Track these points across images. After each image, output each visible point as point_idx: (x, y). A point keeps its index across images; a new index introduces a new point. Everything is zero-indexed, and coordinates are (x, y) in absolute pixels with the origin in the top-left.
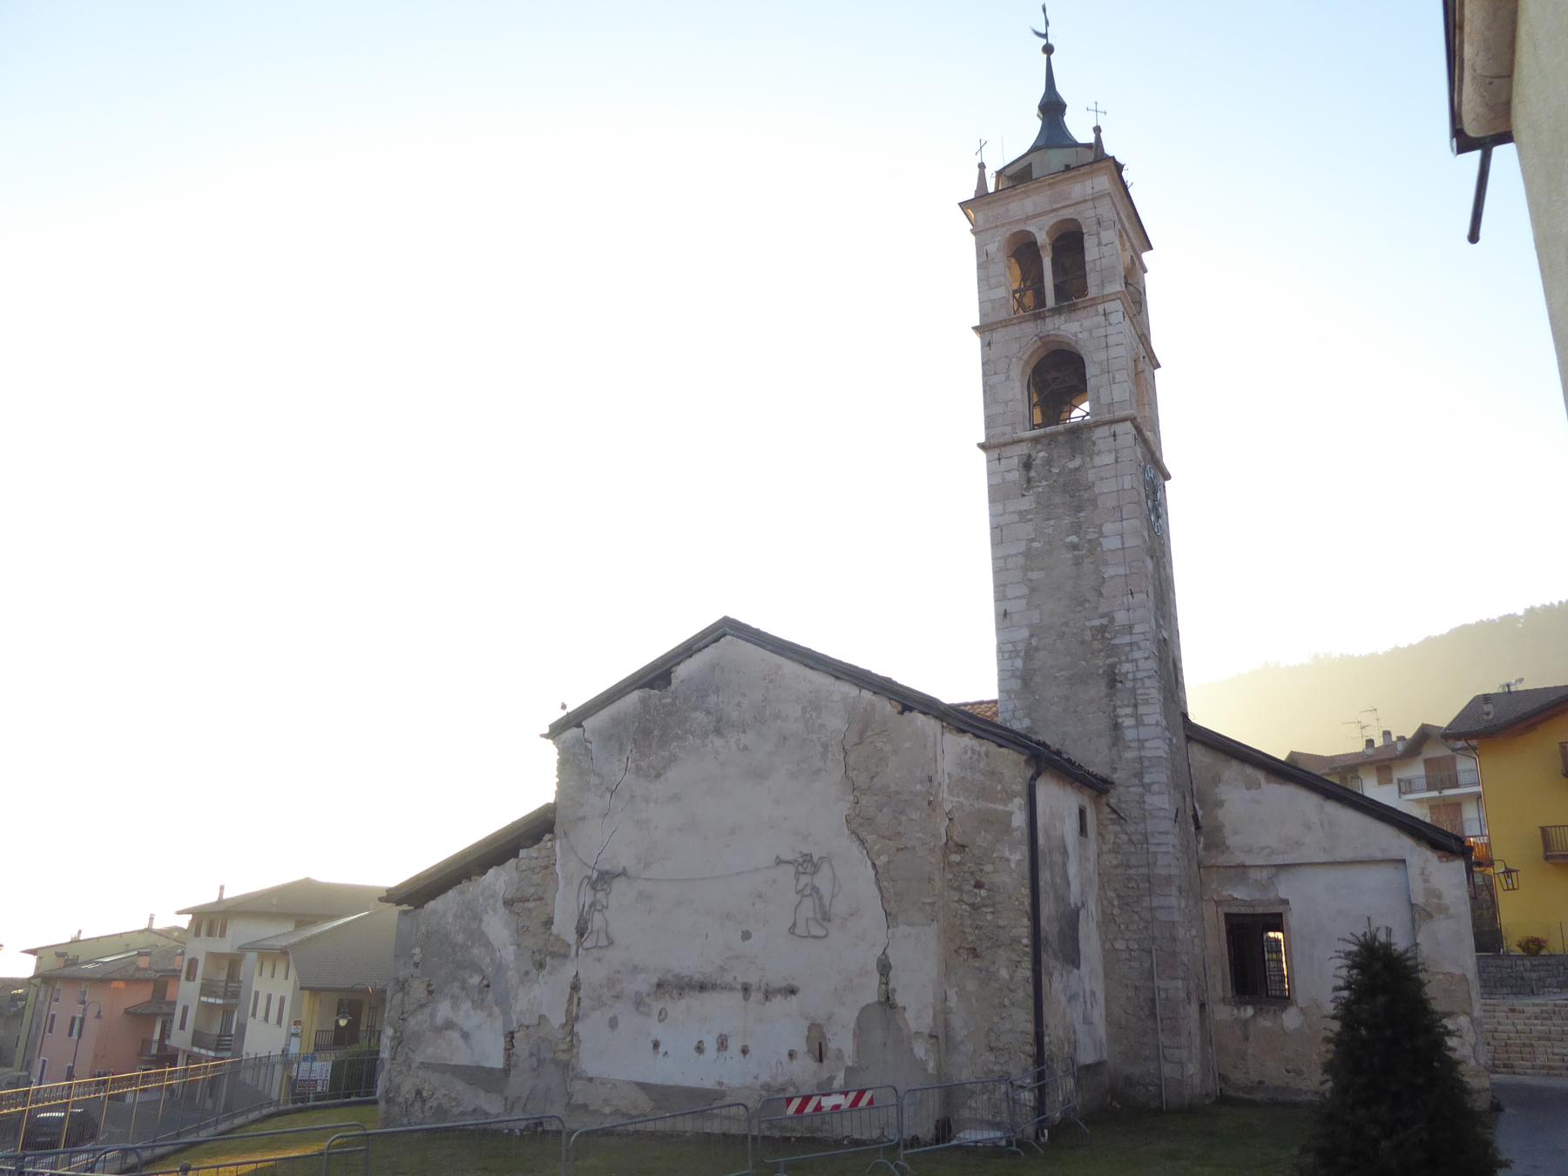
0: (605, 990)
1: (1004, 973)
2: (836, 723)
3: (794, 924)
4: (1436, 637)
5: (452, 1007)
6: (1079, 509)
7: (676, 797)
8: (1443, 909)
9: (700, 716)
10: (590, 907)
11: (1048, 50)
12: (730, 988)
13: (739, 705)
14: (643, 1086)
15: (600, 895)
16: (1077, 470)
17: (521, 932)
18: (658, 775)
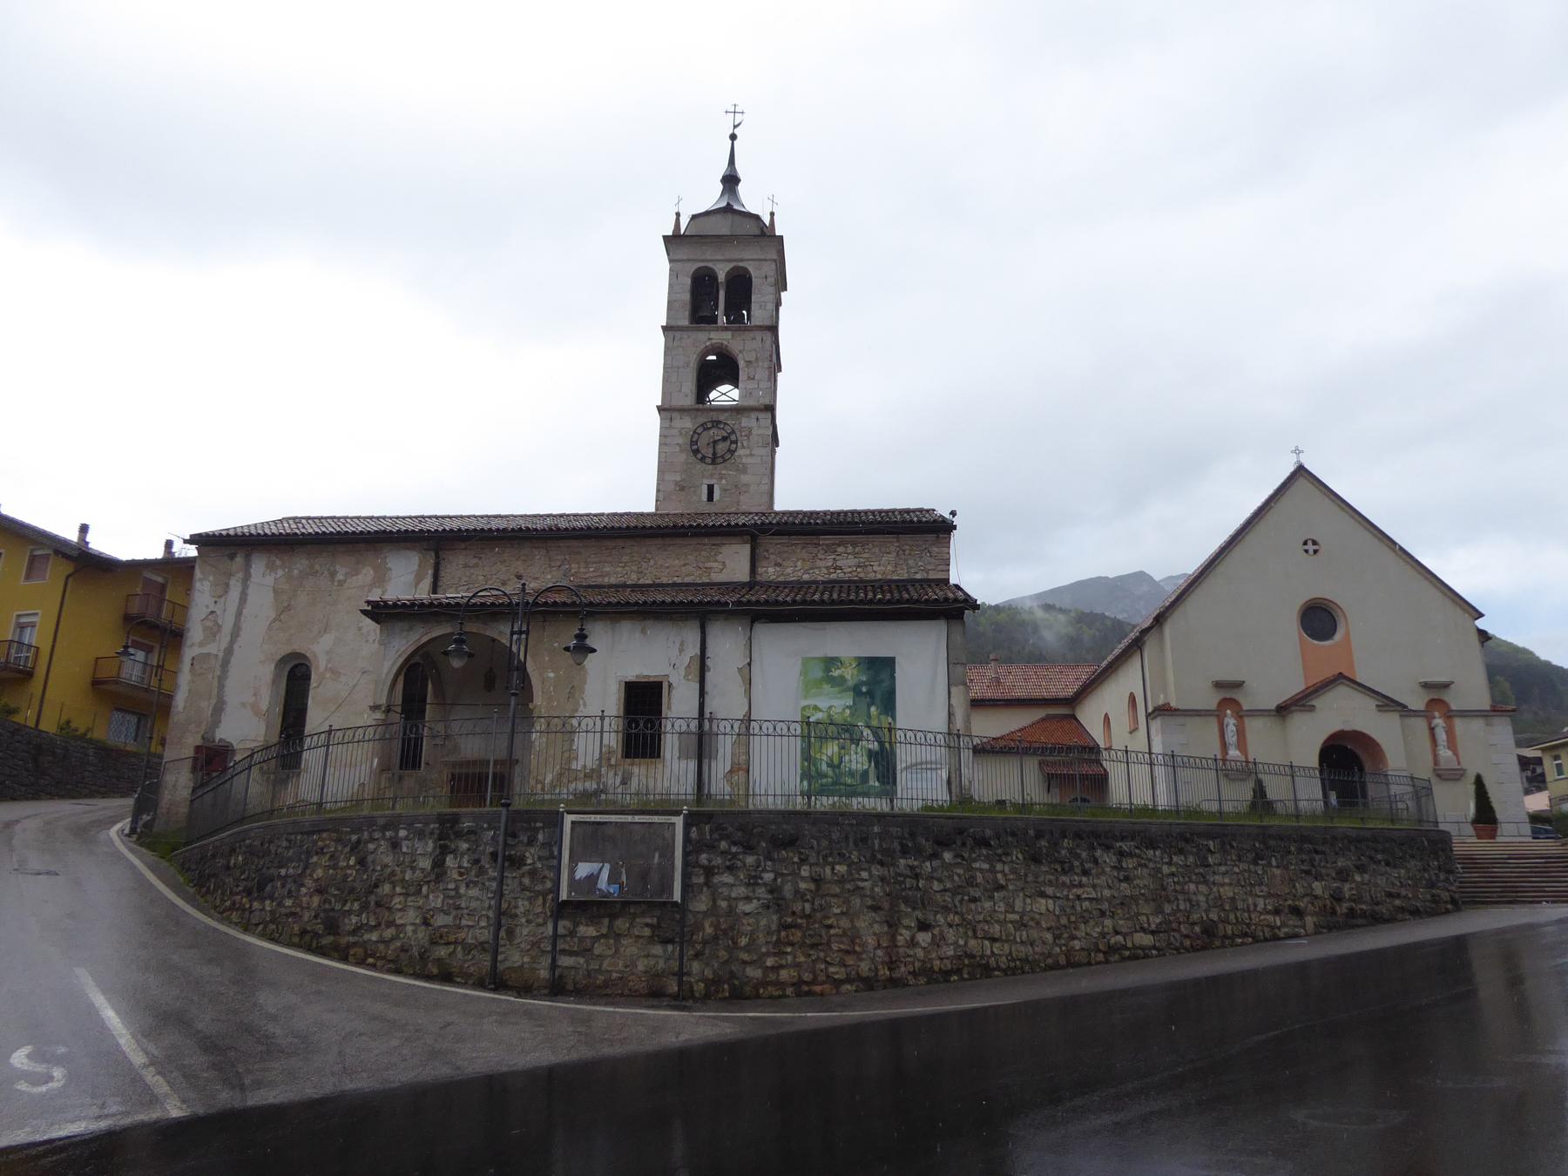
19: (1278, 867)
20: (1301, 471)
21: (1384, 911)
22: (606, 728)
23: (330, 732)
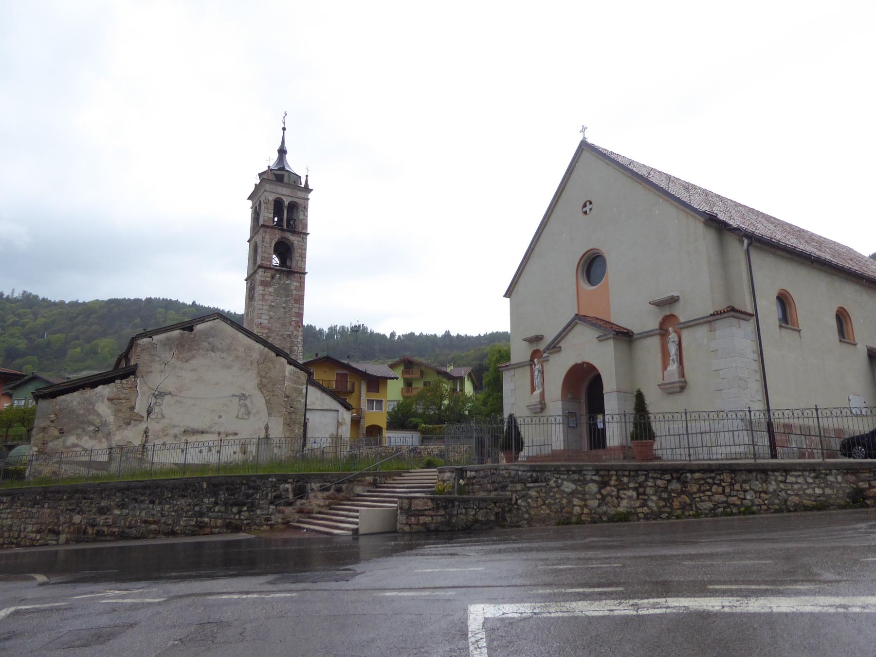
0: (161, 433)
1: (297, 431)
2: (256, 355)
3: (238, 415)
4: (102, 301)
5: (77, 439)
6: (288, 296)
7: (194, 370)
8: (345, 423)
9: (206, 344)
10: (154, 404)
11: (284, 129)
12: (214, 433)
13: (221, 343)
14: (176, 464)
15: (159, 400)
16: (288, 284)
17: (117, 411)
18: (187, 361)
19: (48, 508)
20: (584, 147)
21: (855, 568)
22: (627, 420)
23: (62, 453)
